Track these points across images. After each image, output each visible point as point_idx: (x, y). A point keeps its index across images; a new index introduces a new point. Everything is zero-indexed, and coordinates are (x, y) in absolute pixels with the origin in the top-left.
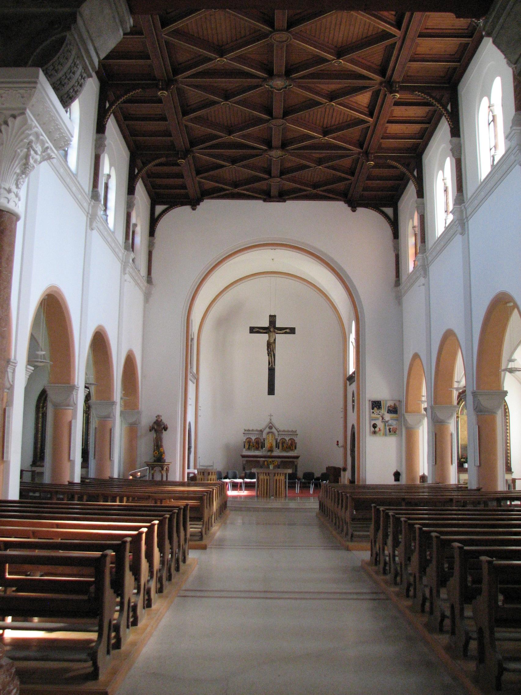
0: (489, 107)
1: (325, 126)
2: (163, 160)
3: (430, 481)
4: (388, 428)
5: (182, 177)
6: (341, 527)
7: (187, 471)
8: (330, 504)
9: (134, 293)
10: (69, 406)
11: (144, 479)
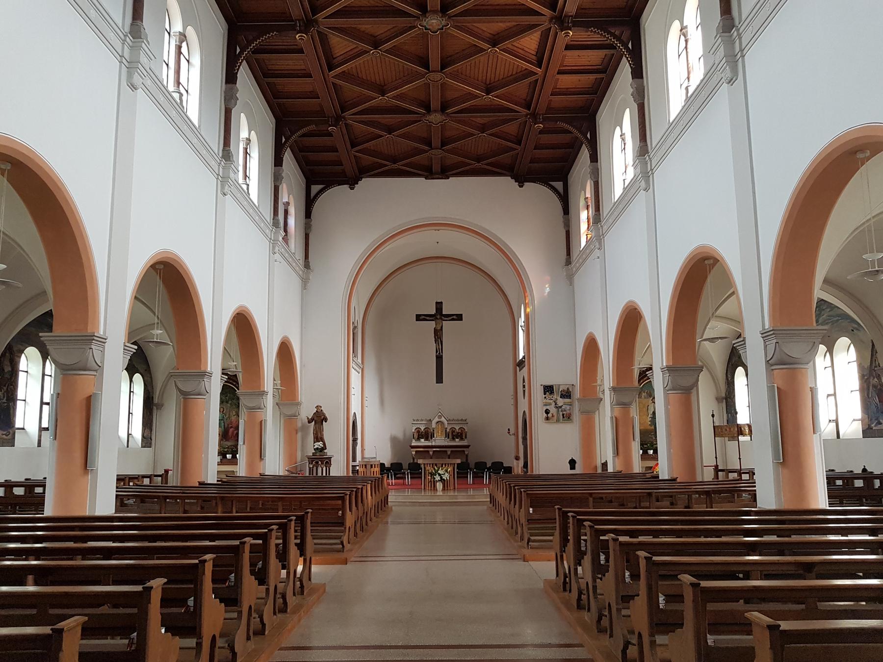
0: (681, 30)
1: (488, 82)
2: (312, 127)
3: (610, 469)
5: (336, 150)
7: (351, 463)
9: (287, 277)
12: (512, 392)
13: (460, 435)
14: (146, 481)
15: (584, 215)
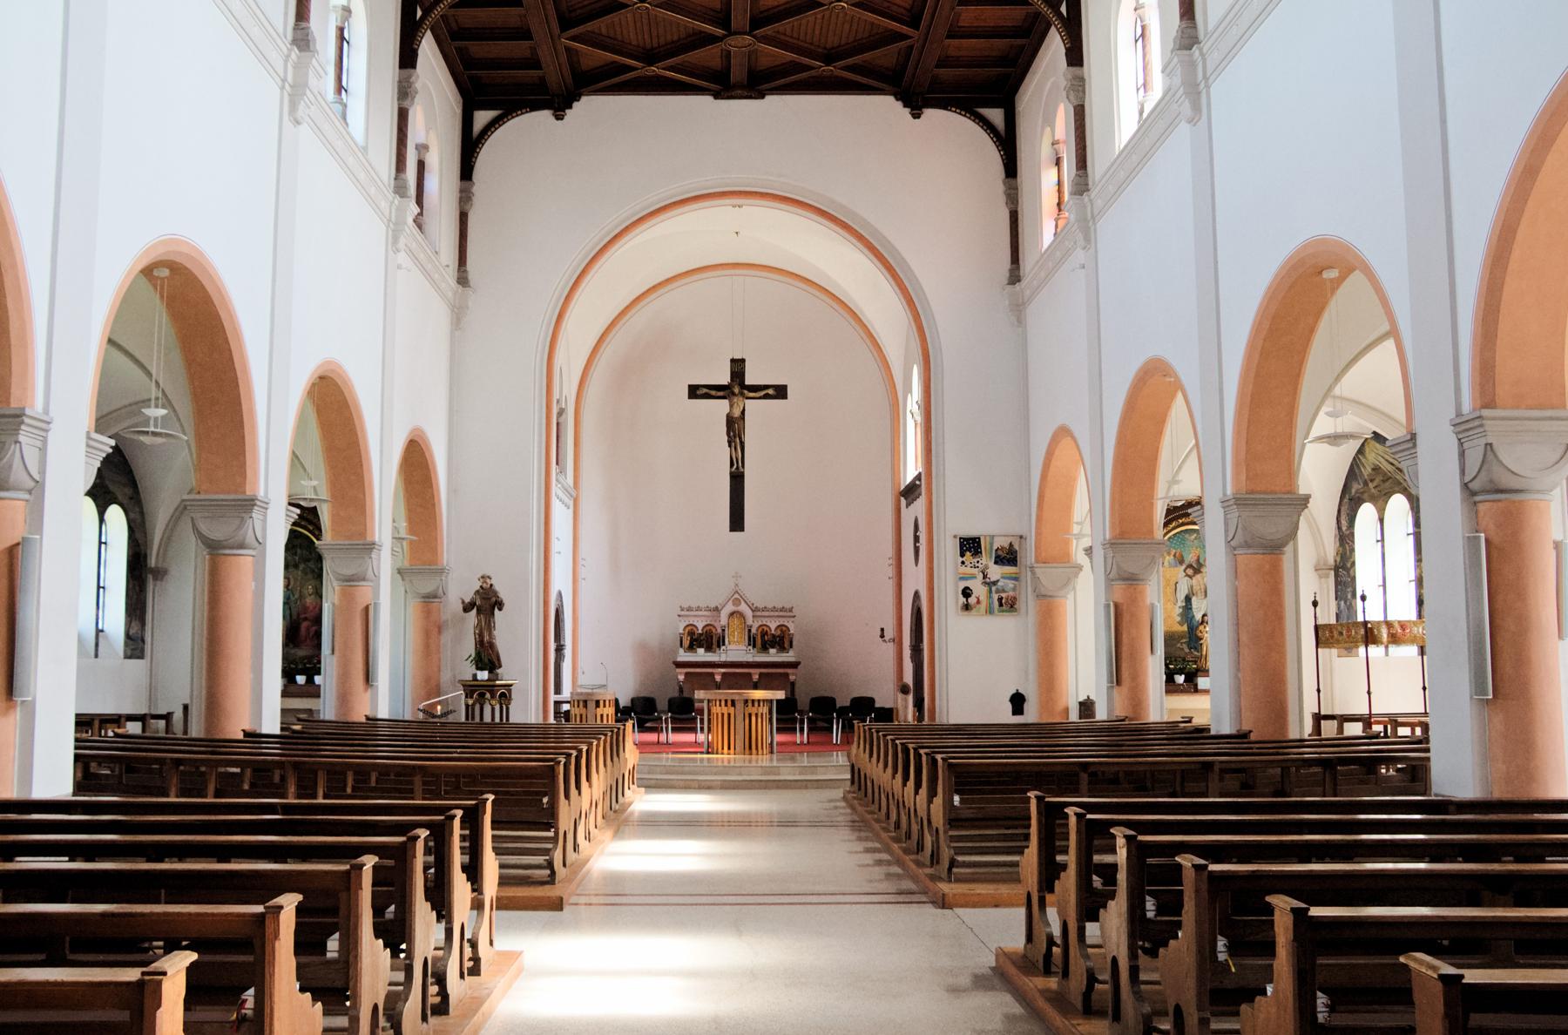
3: (1101, 714)
4: (996, 597)
6: (915, 837)
7: (553, 698)
8: (880, 773)
9: (423, 297)
10: (242, 546)
11: (451, 718)
12: (889, 551)
13: (780, 640)
14: (134, 728)
15: (1049, 177)
